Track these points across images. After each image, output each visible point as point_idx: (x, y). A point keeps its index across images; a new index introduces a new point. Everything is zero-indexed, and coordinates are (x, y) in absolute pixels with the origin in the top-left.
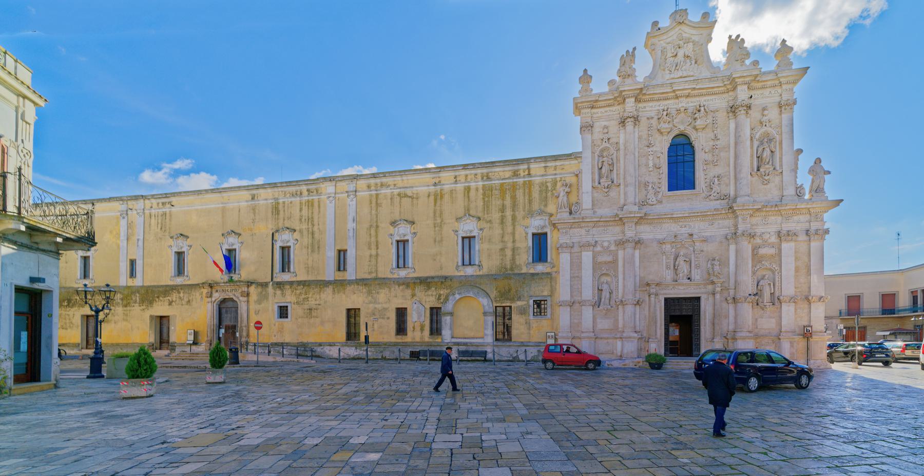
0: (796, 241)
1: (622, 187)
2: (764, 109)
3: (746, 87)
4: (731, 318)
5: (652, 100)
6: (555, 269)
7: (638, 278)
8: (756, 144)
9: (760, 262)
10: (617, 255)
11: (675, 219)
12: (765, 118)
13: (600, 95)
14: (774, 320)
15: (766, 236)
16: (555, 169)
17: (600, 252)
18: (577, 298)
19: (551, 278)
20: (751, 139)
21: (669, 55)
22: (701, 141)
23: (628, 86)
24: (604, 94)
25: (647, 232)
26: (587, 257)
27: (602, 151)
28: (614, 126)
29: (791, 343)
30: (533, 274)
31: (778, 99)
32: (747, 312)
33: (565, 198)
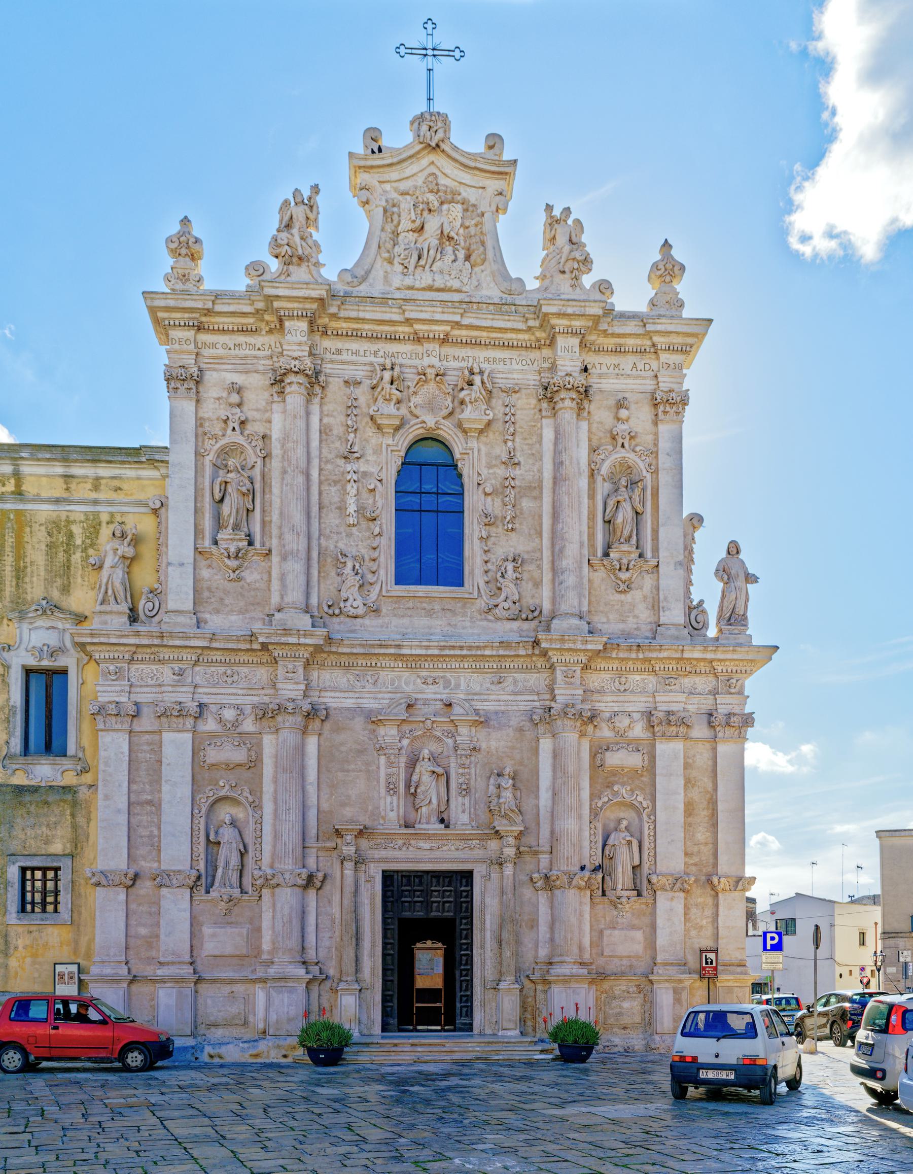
0: (686, 738)
1: (275, 558)
2: (621, 404)
3: (575, 341)
4: (543, 928)
5: (356, 335)
6: (88, 778)
7: (312, 815)
8: (603, 488)
9: (609, 786)
10: (260, 744)
11: (412, 662)
12: (621, 427)
13: (217, 296)
14: (639, 935)
15: (623, 723)
16: (96, 488)
17: (213, 735)
18: (146, 865)
19: (75, 804)
20: (592, 475)
21: (405, 224)
22: (477, 462)
23: (297, 286)
24: (233, 296)
25: (338, 689)
26: (176, 746)
27: (226, 452)
28: (256, 386)
29: (676, 991)
30: (20, 790)
31: (649, 385)
32: (577, 906)
33: (119, 574)
